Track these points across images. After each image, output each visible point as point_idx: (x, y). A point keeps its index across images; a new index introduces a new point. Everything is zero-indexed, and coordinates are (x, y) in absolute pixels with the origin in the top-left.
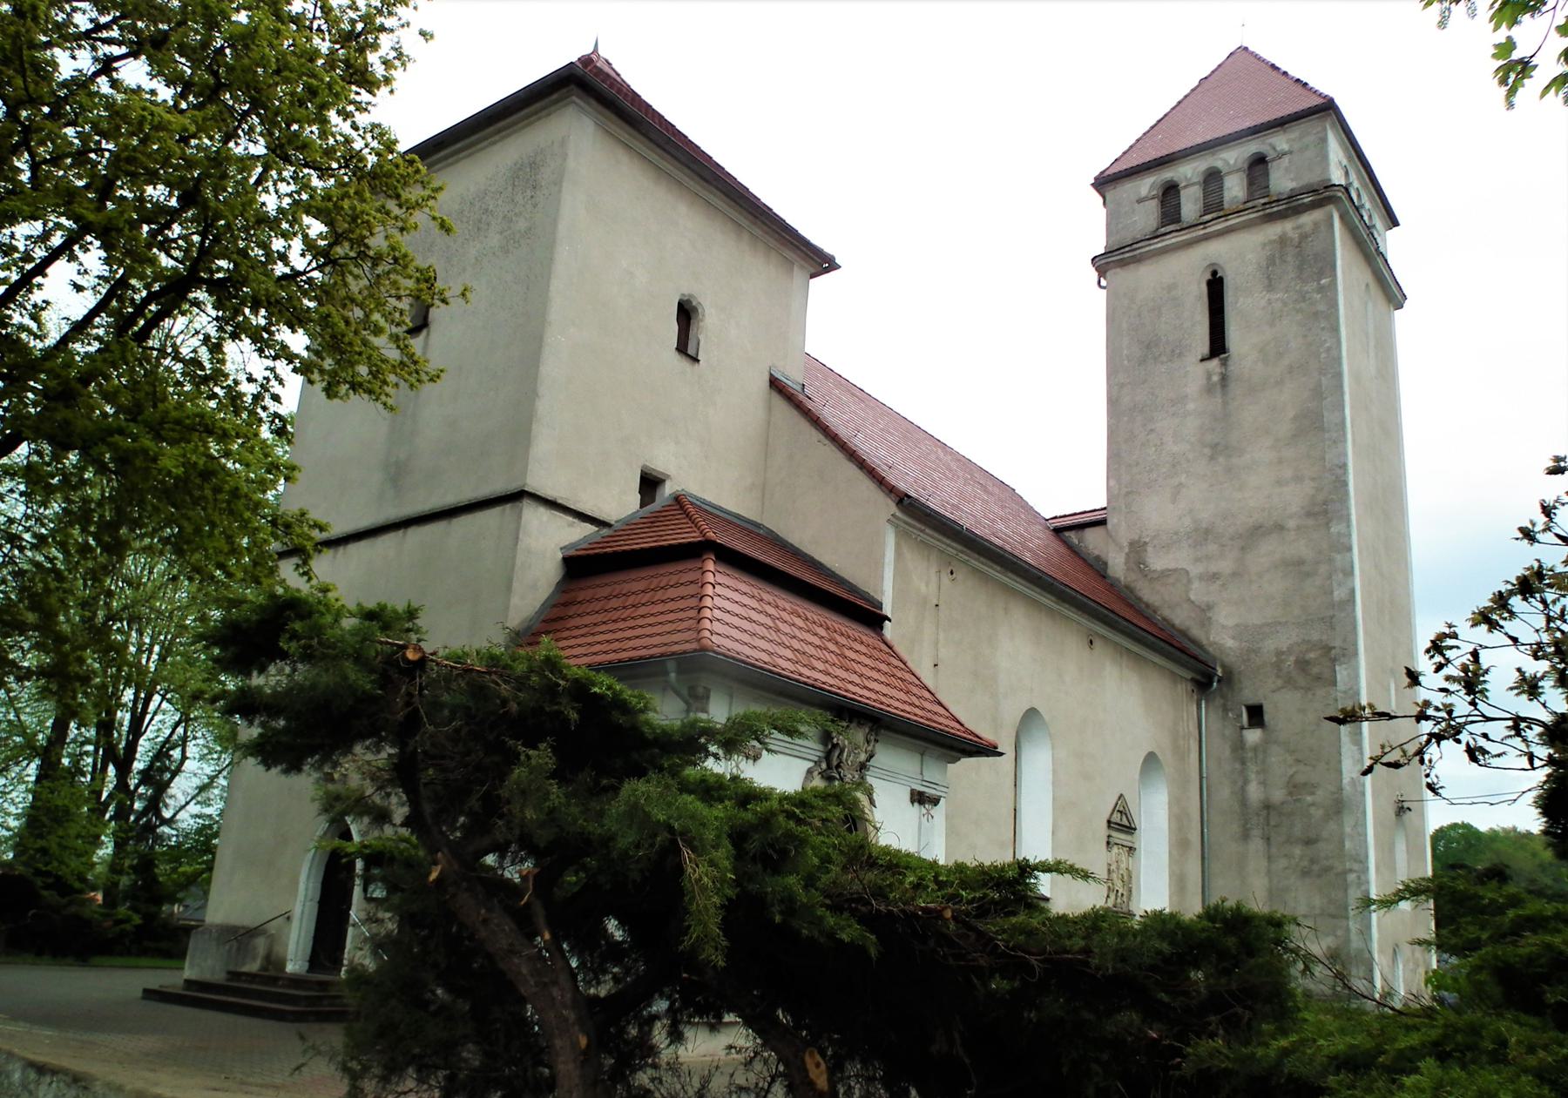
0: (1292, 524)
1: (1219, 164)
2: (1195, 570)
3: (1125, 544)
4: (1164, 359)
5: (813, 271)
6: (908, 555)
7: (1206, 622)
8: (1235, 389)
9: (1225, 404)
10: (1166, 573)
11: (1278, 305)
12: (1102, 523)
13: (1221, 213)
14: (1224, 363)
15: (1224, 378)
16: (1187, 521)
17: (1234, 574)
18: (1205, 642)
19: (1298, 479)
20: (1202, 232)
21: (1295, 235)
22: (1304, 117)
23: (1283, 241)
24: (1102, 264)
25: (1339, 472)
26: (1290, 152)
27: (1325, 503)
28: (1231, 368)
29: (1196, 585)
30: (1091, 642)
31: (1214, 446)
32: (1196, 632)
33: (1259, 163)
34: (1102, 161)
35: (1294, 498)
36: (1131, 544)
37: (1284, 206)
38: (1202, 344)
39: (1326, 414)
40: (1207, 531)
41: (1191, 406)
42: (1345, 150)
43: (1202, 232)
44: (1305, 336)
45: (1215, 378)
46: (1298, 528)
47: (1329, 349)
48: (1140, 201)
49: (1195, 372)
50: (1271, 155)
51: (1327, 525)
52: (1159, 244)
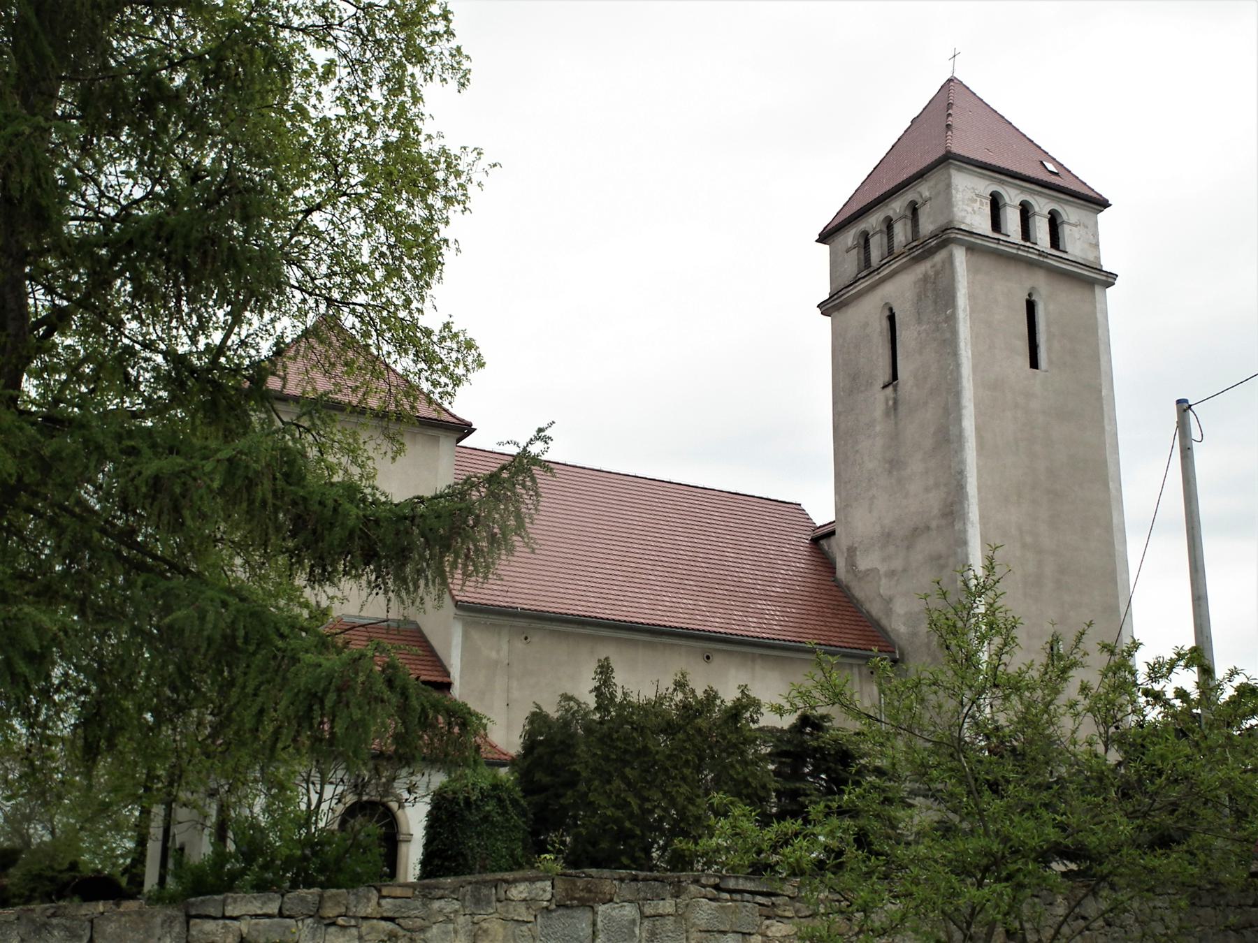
0: (934, 524)
1: (891, 213)
2: (883, 568)
3: (845, 550)
4: (863, 388)
5: (458, 436)
6: (476, 635)
7: (889, 612)
8: (902, 409)
9: (896, 424)
10: (868, 572)
11: (923, 335)
12: (833, 533)
13: (892, 257)
14: (895, 390)
15: (896, 402)
16: (878, 528)
17: (905, 570)
18: (889, 629)
19: (937, 485)
20: (878, 277)
21: (931, 273)
22: (931, 170)
23: (925, 279)
24: (826, 308)
25: (959, 477)
26: (930, 199)
27: (952, 505)
28: (899, 393)
29: (884, 581)
30: (708, 658)
31: (891, 462)
32: (884, 622)
33: (914, 209)
34: (825, 217)
35: (934, 501)
36: (848, 550)
37: (904, 260)
38: (884, 375)
39: (951, 428)
40: (889, 535)
41: (878, 428)
42: (982, 176)
43: (878, 277)
44: (939, 361)
45: (891, 403)
46: (938, 527)
47: (952, 372)
48: (848, 251)
49: (880, 398)
50: (920, 201)
51: (952, 524)
52: (862, 285)
